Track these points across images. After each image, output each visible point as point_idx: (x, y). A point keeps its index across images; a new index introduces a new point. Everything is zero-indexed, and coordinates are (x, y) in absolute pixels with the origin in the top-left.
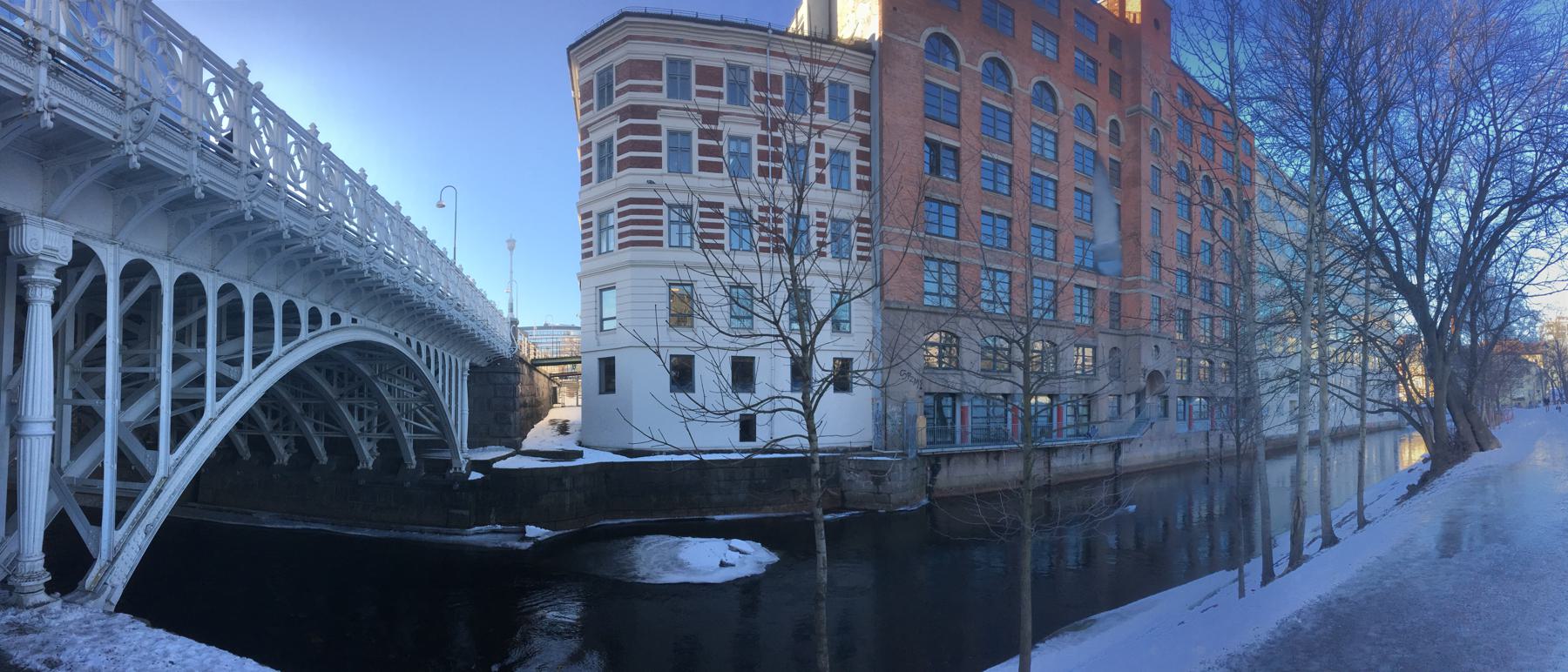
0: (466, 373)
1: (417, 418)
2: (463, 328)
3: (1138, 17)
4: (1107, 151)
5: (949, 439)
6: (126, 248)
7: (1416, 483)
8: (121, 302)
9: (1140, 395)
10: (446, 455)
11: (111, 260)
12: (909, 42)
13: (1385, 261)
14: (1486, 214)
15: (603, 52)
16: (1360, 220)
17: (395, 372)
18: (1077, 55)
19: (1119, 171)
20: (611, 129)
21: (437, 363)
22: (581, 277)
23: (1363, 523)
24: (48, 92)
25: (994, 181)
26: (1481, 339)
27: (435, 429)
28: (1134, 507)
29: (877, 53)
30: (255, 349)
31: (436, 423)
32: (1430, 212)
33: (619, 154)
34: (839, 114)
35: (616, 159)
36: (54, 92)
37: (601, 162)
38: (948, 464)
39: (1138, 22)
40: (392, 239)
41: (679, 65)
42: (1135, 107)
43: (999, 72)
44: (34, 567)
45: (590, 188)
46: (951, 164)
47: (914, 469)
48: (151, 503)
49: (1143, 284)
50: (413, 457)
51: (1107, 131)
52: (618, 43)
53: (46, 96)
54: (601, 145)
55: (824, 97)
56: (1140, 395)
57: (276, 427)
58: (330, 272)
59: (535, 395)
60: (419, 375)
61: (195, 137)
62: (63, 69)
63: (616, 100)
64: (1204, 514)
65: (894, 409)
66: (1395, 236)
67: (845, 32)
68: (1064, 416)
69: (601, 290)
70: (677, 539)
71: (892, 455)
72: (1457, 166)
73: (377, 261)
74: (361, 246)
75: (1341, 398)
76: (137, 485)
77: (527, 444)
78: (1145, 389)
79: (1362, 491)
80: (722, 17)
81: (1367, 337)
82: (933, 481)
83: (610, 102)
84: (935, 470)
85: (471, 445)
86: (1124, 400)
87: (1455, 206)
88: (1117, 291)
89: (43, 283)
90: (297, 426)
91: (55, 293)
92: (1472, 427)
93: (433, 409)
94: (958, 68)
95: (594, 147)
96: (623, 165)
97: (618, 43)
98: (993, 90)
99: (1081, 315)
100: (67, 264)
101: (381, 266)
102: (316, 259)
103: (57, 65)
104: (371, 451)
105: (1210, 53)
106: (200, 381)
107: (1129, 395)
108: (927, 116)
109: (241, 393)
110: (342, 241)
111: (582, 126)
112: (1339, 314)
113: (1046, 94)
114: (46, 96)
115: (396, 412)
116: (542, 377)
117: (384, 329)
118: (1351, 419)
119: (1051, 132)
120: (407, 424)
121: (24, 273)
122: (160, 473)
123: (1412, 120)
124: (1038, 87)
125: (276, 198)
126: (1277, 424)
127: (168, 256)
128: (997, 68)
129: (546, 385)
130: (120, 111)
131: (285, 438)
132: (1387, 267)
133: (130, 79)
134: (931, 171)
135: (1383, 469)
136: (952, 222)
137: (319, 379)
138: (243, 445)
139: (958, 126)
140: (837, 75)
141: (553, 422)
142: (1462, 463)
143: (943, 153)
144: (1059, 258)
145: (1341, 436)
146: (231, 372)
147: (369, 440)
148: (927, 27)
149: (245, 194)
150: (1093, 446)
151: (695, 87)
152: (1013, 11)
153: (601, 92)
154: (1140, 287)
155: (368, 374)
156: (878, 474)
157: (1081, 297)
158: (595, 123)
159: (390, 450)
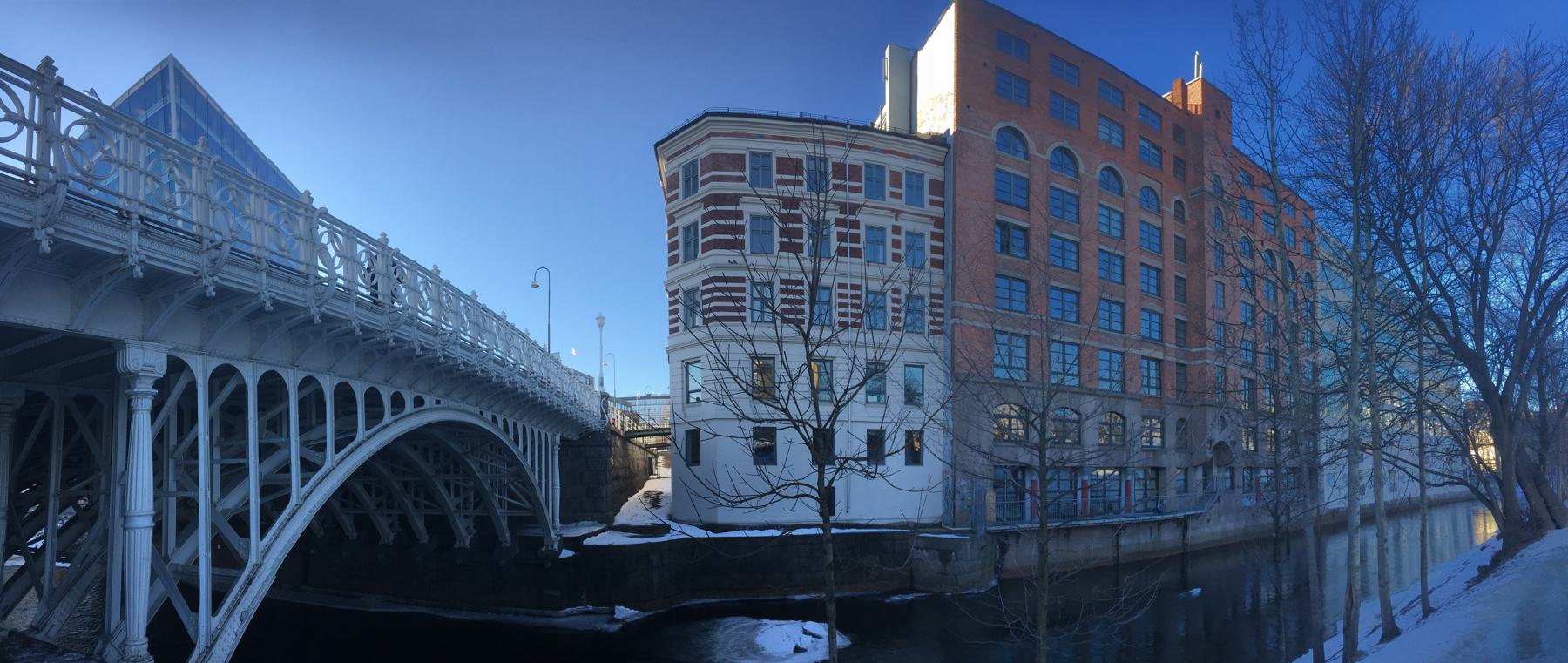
0: (557, 447)
1: (512, 495)
2: (548, 404)
3: (1199, 109)
4: (1172, 229)
5: (1019, 515)
6: (213, 356)
7: (1488, 564)
8: (210, 404)
9: (1207, 468)
10: (535, 532)
11: (200, 367)
12: (981, 135)
13: (1442, 326)
14: (1545, 276)
15: (689, 147)
16: (1413, 286)
17: (487, 448)
18: (1142, 143)
19: (1184, 247)
20: (697, 215)
21: (525, 439)
22: (669, 351)
23: (1428, 611)
24: (138, 249)
25: (1063, 258)
26: (1551, 406)
27: (528, 505)
28: (1199, 590)
29: (952, 146)
30: (337, 432)
31: (529, 499)
32: (1486, 276)
33: (703, 237)
34: (915, 198)
35: (701, 241)
36: (144, 248)
37: (687, 244)
38: (1017, 542)
39: (1199, 113)
40: (500, 342)
41: (874, 169)
42: (1199, 188)
43: (1066, 159)
44: (139, 651)
45: (677, 268)
46: (1022, 243)
47: (983, 548)
48: (244, 590)
49: (1208, 354)
50: (508, 535)
51: (1172, 210)
52: (702, 140)
53: (137, 253)
54: (687, 229)
55: (901, 184)
56: (1207, 468)
57: (380, 505)
58: (409, 359)
59: (629, 467)
60: (503, 450)
61: (264, 260)
62: (150, 229)
63: (701, 190)
64: (1273, 595)
65: (963, 483)
66: (1450, 301)
67: (924, 127)
68: (1132, 491)
69: (688, 364)
70: (755, 622)
71: (961, 533)
72: (1510, 233)
73: (452, 347)
74: (436, 335)
75: (1404, 469)
76: (233, 572)
77: (620, 519)
78: (1211, 462)
79: (1426, 574)
80: (801, 114)
81: (1421, 404)
82: (1002, 559)
83: (695, 191)
84: (1004, 550)
85: (565, 521)
86: (1190, 472)
87: (1511, 269)
88: (1182, 362)
89: (143, 394)
90: (399, 504)
91: (153, 401)
92: (1546, 502)
93: (523, 484)
94: (1027, 157)
95: (680, 231)
96: (706, 247)
97: (702, 140)
98: (1061, 176)
99: (1148, 386)
100: (162, 376)
101: (457, 352)
102: (393, 348)
103: (146, 227)
104: (467, 529)
105: (1249, 133)
106: (286, 469)
107: (1195, 467)
108: (997, 200)
109: (325, 477)
110: (416, 332)
111: (669, 213)
112: (1394, 380)
113: (1113, 179)
114: (137, 253)
115: (488, 487)
116: (637, 449)
117: (471, 409)
118: (1413, 490)
119: (1118, 212)
120: (500, 501)
121: (129, 387)
122: (253, 559)
123: (1463, 190)
124: (1105, 172)
125: (347, 301)
126: (1333, 493)
127: (250, 359)
128: (1065, 157)
129: (641, 456)
130: (198, 252)
131: (389, 515)
132: (1444, 332)
133: (206, 226)
134: (1002, 249)
135: (1456, 544)
136: (1023, 296)
137: (415, 457)
138: (419, 525)
139: (1027, 209)
140: (913, 165)
141: (647, 495)
142: (1536, 543)
143: (1014, 233)
144: (1126, 331)
145: (1397, 511)
146: (314, 457)
147: (466, 517)
148: (997, 122)
149: (313, 301)
150: (1160, 523)
151: (775, 176)
152: (1078, 105)
153: (687, 182)
154: (1205, 358)
155: (458, 450)
156: (945, 553)
157: (1149, 369)
158: (681, 210)
159: (484, 525)
